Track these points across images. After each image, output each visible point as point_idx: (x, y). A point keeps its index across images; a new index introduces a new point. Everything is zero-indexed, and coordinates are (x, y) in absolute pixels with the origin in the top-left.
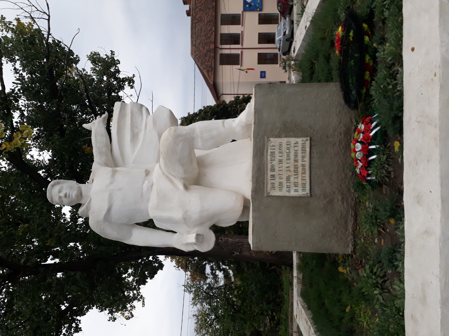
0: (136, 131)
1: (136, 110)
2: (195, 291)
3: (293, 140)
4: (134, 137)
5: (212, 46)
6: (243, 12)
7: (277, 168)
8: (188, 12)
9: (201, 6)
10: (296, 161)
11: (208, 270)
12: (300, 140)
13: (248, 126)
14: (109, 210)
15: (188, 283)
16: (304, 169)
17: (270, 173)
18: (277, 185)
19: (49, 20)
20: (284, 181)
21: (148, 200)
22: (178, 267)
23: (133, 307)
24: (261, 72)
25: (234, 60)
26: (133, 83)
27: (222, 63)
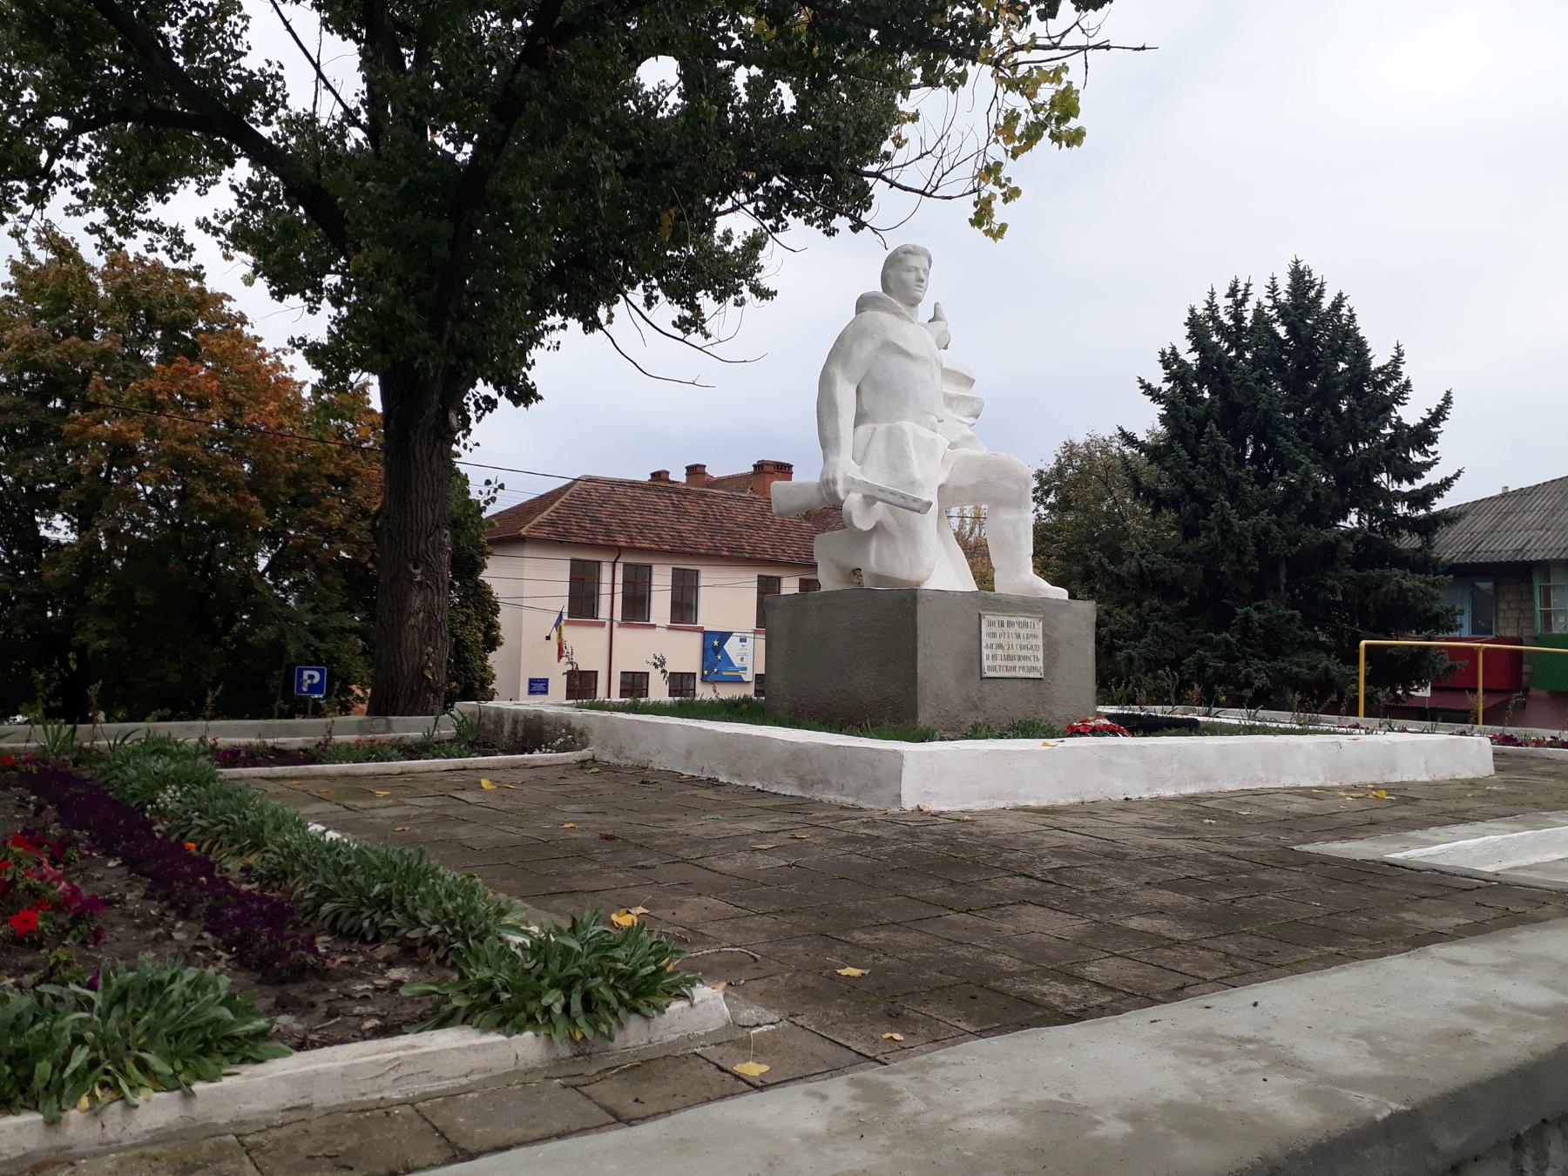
3: (1040, 654)
5: (622, 541)
6: (700, 630)
7: (1011, 630)
12: (1040, 664)
17: (1005, 619)
19: (922, 193)
24: (546, 681)
25: (582, 604)
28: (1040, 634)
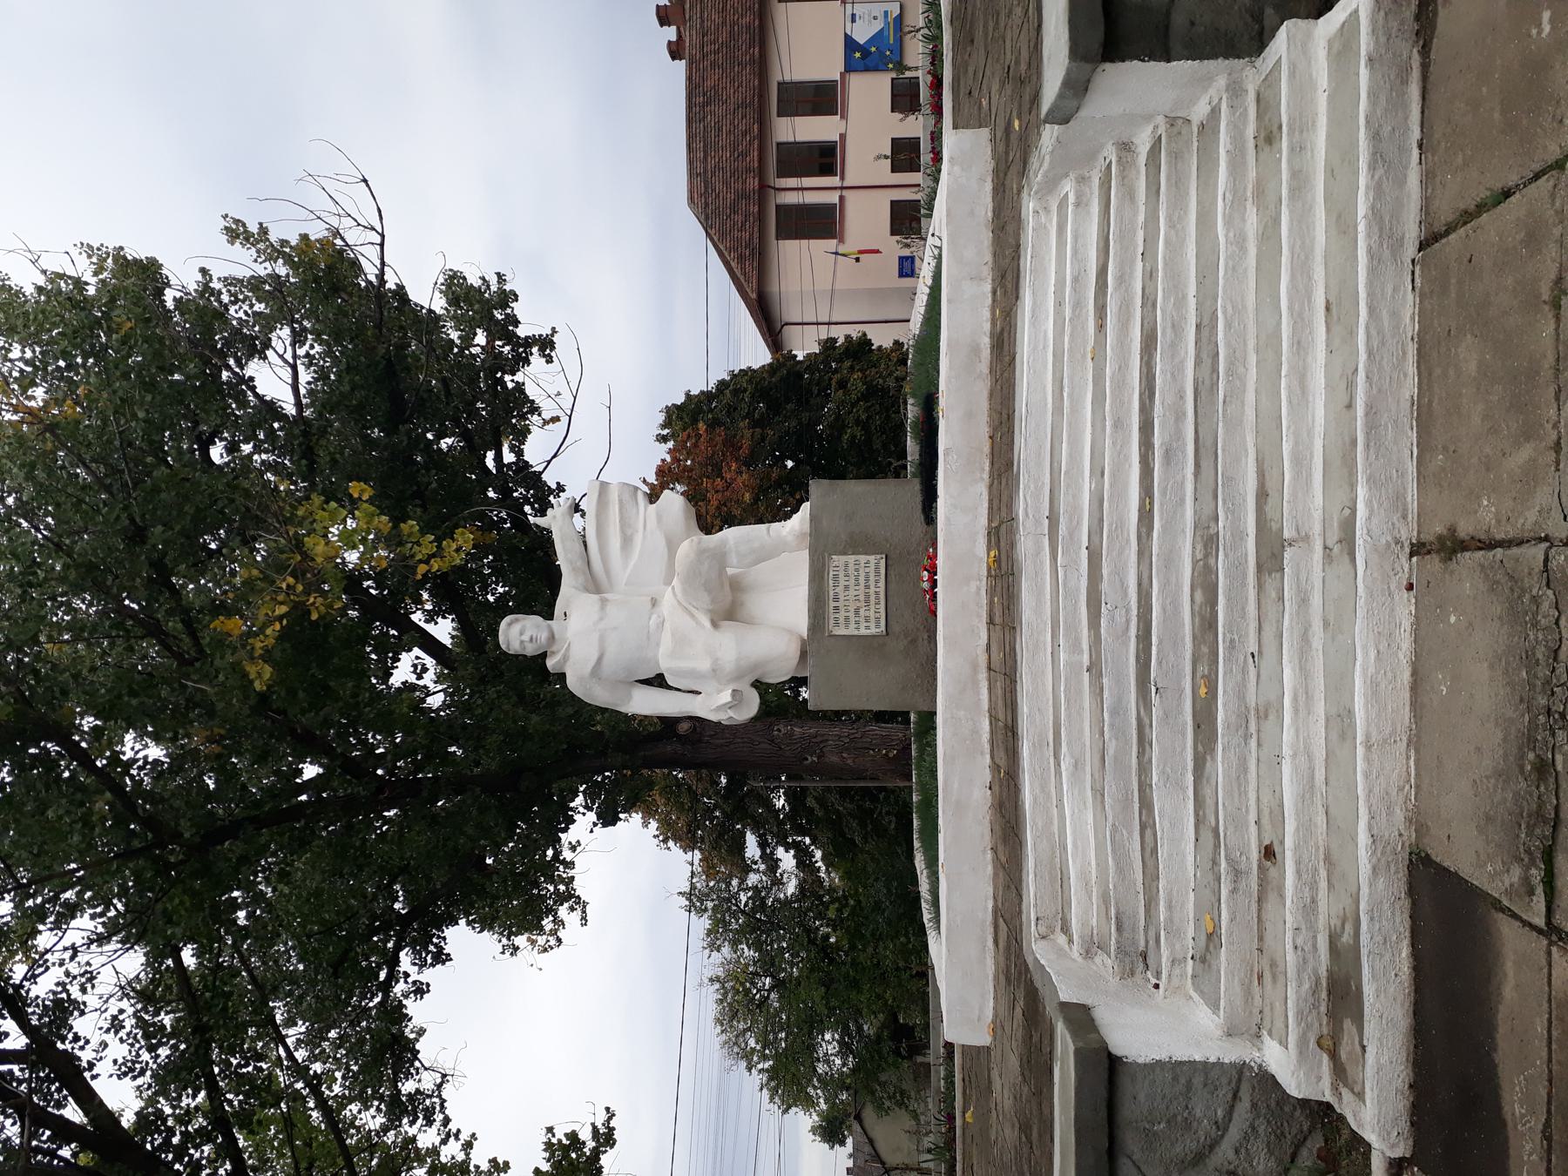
0: (629, 532)
1: (627, 496)
2: (715, 909)
3: (863, 558)
4: (627, 541)
5: (753, 183)
7: (842, 598)
8: (674, 48)
9: (716, 52)
10: (867, 587)
11: (752, 848)
12: (872, 558)
13: (802, 535)
14: (600, 659)
15: (693, 887)
16: (877, 598)
17: (832, 604)
18: (842, 620)
19: (382, 245)
20: (851, 614)
21: (658, 645)
22: (665, 841)
23: (559, 923)
25: (820, 223)
26: (553, 348)
27: (785, 233)
28: (843, 558)
